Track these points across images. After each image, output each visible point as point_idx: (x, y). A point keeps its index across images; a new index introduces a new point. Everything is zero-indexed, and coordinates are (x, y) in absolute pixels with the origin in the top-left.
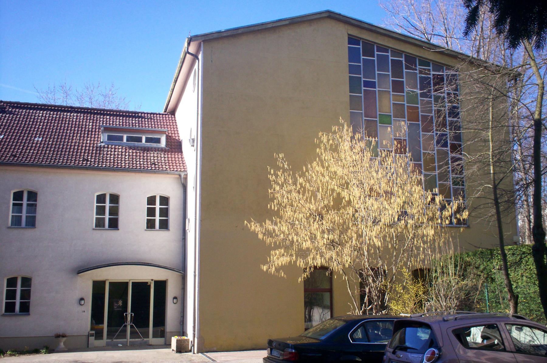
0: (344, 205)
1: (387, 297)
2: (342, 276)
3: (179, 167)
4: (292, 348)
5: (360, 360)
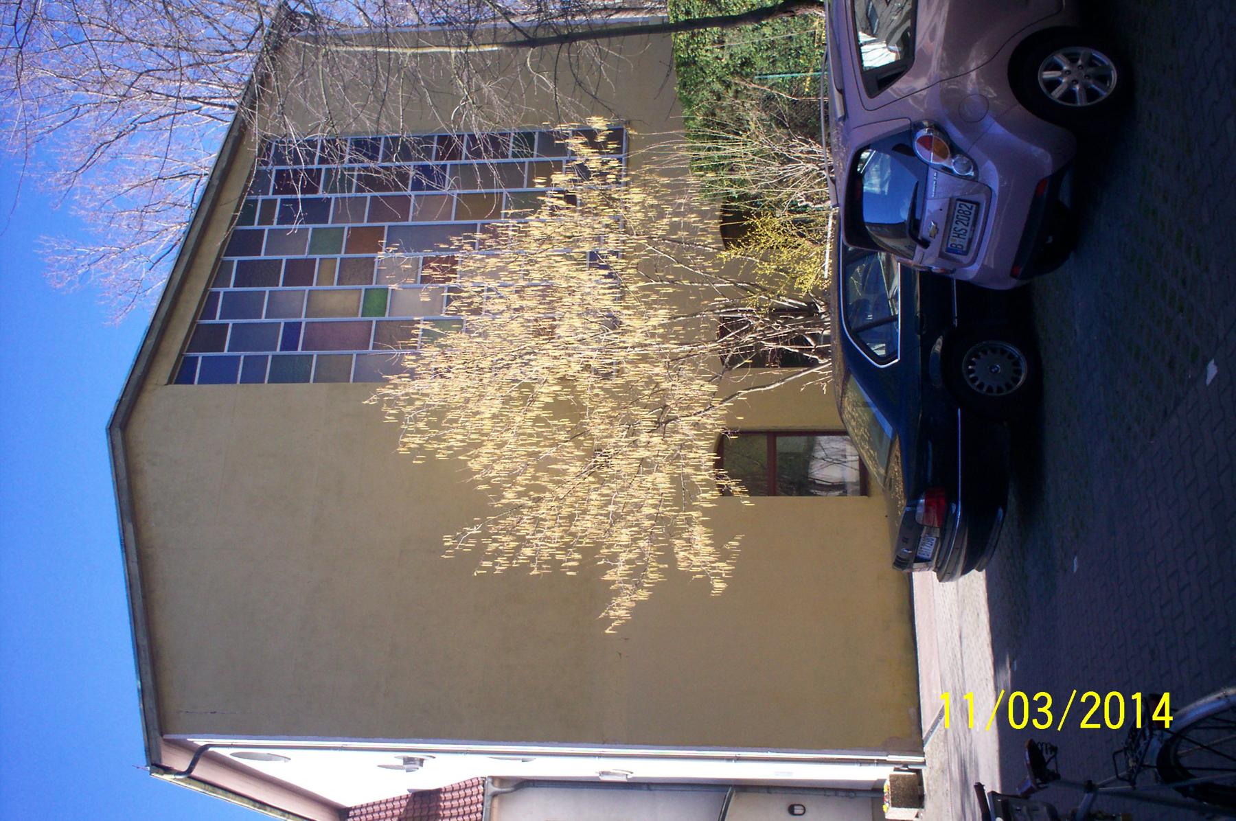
0: (572, 393)
1: (787, 302)
2: (736, 402)
3: (474, 799)
4: (916, 505)
5: (940, 340)
